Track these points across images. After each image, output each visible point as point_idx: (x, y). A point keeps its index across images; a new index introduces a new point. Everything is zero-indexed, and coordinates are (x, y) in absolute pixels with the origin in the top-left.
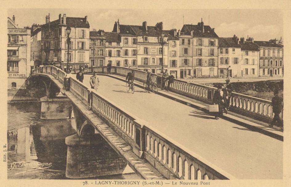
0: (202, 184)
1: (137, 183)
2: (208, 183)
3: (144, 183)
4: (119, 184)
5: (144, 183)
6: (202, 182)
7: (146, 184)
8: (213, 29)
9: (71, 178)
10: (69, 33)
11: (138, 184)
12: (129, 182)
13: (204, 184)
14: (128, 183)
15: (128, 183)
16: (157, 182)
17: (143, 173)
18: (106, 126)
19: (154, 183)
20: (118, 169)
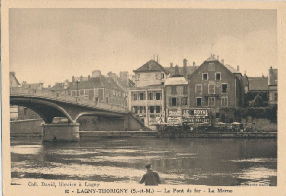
0: (176, 191)
1: (93, 191)
2: (182, 191)
3: (133, 191)
4: (104, 192)
5: (133, 191)
6: (175, 190)
7: (134, 192)
8: (263, 76)
9: (16, 143)
10: (248, 84)
11: (126, 192)
12: (115, 190)
13: (178, 191)
14: (114, 191)
15: (114, 191)
16: (220, 190)
17: (143, 76)
18: (214, 136)
19: (143, 191)
20: (147, 69)
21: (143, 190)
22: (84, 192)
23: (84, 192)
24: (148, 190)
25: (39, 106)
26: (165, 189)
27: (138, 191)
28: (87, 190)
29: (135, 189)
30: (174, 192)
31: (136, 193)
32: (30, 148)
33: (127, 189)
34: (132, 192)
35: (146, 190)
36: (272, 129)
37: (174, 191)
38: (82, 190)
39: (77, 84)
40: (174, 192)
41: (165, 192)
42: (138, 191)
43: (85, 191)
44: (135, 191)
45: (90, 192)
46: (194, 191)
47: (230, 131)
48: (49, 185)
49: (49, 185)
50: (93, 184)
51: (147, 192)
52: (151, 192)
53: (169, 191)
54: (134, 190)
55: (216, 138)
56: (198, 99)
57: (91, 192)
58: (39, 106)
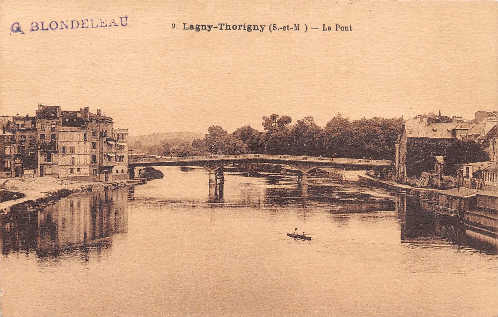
7: (275, 29)
21: (288, 26)
24: (297, 26)
26: (324, 25)
27: (281, 28)
29: (276, 25)
30: (337, 30)
31: (277, 30)
32: (496, 179)
33: (264, 26)
34: (272, 30)
35: (293, 27)
36: (494, 221)
37: (337, 28)
39: (21, 31)
40: (337, 30)
42: (281, 28)
44: (274, 26)
47: (269, 167)
50: (251, 26)
53: (329, 28)
54: (274, 26)
55: (144, 157)
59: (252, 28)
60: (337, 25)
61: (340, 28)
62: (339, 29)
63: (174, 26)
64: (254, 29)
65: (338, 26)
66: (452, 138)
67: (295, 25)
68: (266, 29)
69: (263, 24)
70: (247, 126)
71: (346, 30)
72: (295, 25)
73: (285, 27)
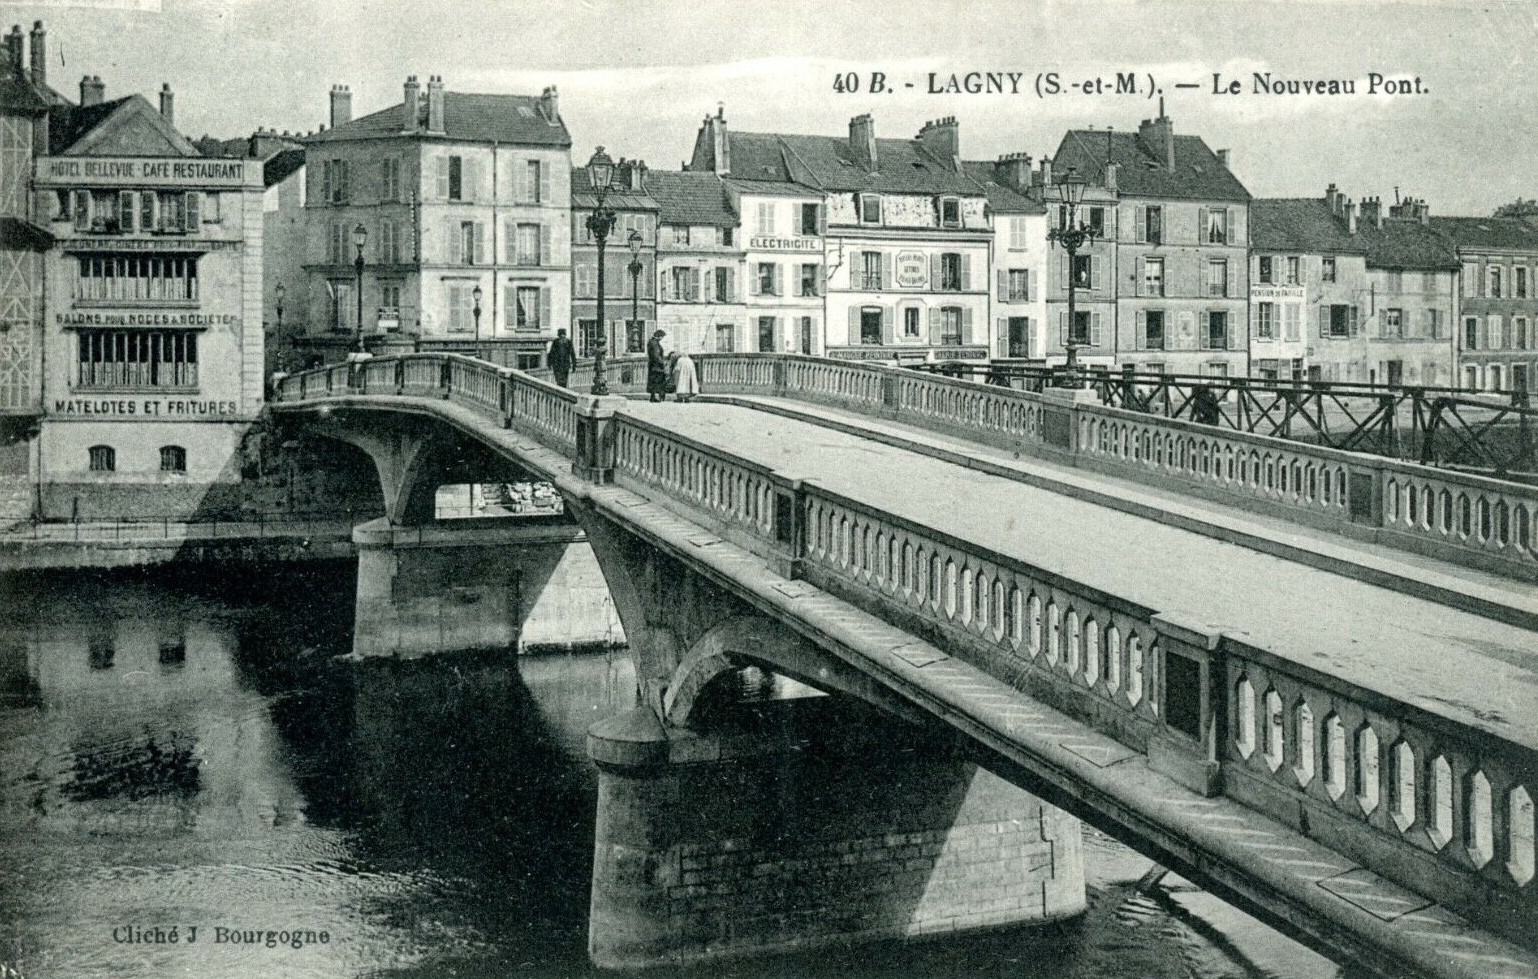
2: (1413, 86)
3: (1043, 84)
5: (1043, 84)
7: (1054, 88)
11: (1015, 91)
21: (1099, 82)
22: (962, 87)
23: (962, 87)
24: (1126, 78)
25: (1524, 230)
26: (932, 76)
28: (978, 75)
29: (1056, 76)
31: (1061, 93)
33: (1020, 75)
34: (1043, 91)
35: (1114, 81)
38: (953, 77)
41: (931, 91)
43: (1275, 86)
45: (993, 87)
46: (524, 221)
48: (1308, 91)
49: (1308, 91)
51: (1118, 91)
52: (1137, 89)
56: (1516, 368)
57: (1000, 88)
58: (1524, 230)
59: (303, 938)
60: (1372, 76)
61: (1383, 85)
62: (1379, 89)
63: (890, 91)
64: (308, 941)
65: (1376, 80)
66: (520, 645)
67: (1120, 76)
68: (1026, 85)
69: (1015, 71)
70: (158, 454)
71: (1402, 91)
72: (1120, 76)
73: (1088, 84)
